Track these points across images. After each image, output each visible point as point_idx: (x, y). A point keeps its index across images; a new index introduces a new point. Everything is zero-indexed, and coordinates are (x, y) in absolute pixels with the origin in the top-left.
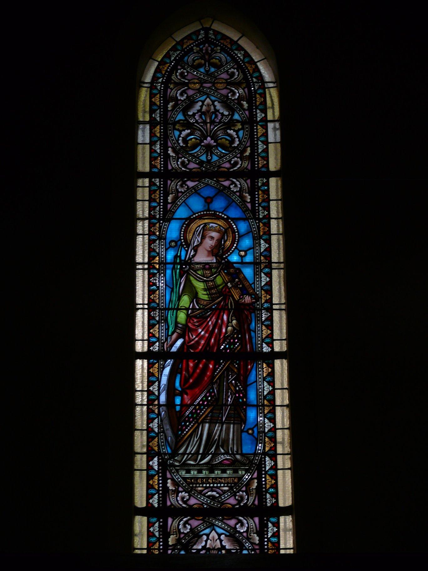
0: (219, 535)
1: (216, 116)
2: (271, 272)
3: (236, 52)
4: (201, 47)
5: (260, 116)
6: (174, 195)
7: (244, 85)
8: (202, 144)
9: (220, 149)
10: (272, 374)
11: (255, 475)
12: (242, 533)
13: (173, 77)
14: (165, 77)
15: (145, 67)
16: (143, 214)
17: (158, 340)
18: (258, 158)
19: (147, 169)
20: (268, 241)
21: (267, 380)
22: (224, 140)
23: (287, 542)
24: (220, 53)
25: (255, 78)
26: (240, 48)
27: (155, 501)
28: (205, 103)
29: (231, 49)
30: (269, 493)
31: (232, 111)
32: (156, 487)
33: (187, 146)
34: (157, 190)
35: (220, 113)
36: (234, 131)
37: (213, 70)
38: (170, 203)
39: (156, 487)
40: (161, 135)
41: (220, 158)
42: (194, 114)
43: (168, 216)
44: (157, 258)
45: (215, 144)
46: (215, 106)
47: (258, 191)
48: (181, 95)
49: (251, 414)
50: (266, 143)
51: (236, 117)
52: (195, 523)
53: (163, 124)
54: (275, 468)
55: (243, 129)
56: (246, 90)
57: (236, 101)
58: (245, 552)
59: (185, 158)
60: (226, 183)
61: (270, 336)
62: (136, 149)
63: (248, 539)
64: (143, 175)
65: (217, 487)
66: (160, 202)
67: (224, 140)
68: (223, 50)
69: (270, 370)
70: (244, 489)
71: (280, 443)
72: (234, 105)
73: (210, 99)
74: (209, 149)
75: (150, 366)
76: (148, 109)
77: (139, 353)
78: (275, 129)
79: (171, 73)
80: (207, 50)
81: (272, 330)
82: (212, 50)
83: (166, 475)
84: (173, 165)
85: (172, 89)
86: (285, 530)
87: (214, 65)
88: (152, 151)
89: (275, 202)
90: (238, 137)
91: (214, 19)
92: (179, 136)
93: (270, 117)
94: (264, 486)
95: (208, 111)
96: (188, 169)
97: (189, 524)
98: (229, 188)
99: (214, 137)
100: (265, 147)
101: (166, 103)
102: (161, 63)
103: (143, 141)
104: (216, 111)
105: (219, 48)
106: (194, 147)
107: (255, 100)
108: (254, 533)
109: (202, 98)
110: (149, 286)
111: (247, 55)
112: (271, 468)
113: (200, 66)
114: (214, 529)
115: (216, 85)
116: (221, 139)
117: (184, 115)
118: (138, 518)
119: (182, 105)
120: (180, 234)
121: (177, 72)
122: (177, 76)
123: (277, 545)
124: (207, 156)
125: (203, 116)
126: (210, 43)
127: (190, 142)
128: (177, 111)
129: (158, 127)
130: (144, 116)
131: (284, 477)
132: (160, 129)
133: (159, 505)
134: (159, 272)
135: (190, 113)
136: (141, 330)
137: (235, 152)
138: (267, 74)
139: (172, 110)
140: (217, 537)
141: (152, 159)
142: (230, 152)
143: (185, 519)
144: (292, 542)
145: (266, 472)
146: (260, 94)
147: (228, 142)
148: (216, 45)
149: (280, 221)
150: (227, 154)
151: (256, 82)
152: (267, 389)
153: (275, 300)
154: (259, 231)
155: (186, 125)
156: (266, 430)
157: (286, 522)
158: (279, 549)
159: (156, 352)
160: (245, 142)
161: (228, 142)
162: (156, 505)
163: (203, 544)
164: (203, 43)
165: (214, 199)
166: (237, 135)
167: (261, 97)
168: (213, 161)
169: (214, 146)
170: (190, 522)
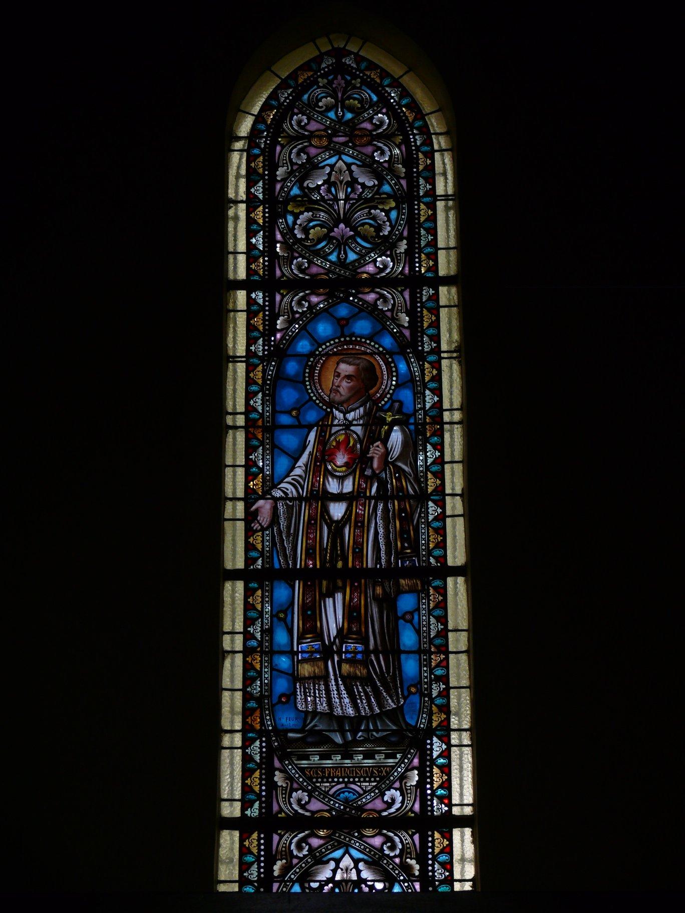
0: (356, 862)
4: (331, 78)
5: (423, 186)
6: (284, 861)
7: (399, 139)
12: (392, 858)
14: (268, 136)
18: (433, 866)
19: (240, 565)
22: (367, 227)
23: (465, 872)
28: (342, 865)
29: (381, 85)
30: (438, 766)
32: (255, 851)
33: (307, 238)
37: (349, 116)
39: (255, 851)
40: (264, 222)
45: (352, 233)
46: (359, 872)
48: (299, 303)
58: (397, 889)
61: (448, 850)
63: (395, 320)
64: (235, 575)
67: (367, 227)
72: (383, 171)
75: (249, 592)
76: (243, 172)
77: (229, 570)
78: (447, 209)
81: (440, 396)
83: (275, 235)
85: (283, 147)
86: (463, 860)
87: (351, 109)
89: (444, 251)
90: (389, 220)
92: (295, 223)
93: (440, 190)
96: (307, 811)
97: (307, 844)
98: (375, 304)
105: (359, 80)
107: (416, 169)
108: (411, 859)
109: (333, 160)
114: (340, 158)
121: (291, 119)
122: (292, 125)
123: (442, 560)
124: (339, 253)
125: (333, 190)
127: (312, 231)
129: (261, 208)
130: (232, 722)
131: (454, 527)
132: (264, 212)
134: (262, 390)
140: (345, 168)
141: (252, 159)
143: (300, 836)
144: (468, 719)
145: (428, 524)
146: (440, 767)
148: (355, 77)
152: (435, 627)
157: (463, 842)
158: (450, 805)
159: (255, 818)
161: (372, 229)
165: (351, 321)
166: (387, 217)
167: (433, 368)
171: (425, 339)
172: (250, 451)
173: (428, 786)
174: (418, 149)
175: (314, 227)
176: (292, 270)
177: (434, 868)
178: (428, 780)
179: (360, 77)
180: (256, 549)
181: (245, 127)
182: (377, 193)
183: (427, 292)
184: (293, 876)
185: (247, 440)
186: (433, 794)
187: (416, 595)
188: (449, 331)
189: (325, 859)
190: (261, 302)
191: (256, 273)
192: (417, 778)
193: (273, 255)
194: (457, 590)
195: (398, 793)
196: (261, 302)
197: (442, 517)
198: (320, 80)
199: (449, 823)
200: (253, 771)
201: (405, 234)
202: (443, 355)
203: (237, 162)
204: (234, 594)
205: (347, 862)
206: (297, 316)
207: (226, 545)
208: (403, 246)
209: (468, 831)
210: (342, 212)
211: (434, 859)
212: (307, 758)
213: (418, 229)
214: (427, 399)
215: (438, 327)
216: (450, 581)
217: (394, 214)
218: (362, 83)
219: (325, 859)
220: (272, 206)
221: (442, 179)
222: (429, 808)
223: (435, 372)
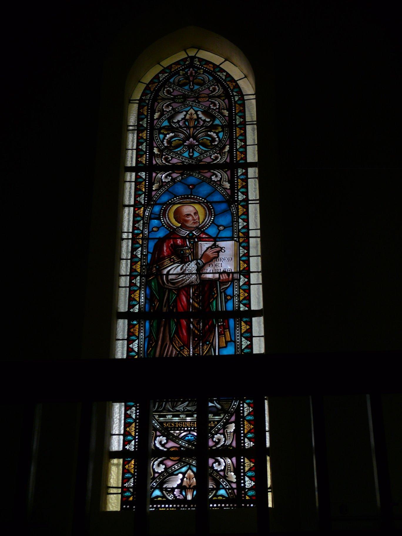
1: (199, 123)
4: (186, 70)
13: (160, 94)
16: (131, 164)
18: (237, 180)
21: (242, 245)
23: (259, 347)
24: (203, 74)
25: (236, 92)
28: (189, 113)
31: (213, 118)
33: (171, 146)
34: (140, 234)
35: (202, 120)
37: (196, 87)
42: (178, 122)
45: (197, 143)
46: (198, 115)
47: (238, 185)
51: (217, 122)
52: (169, 463)
53: (149, 131)
54: (248, 284)
57: (217, 110)
59: (170, 88)
60: (208, 175)
69: (245, 210)
74: (191, 147)
77: (115, 458)
79: (159, 90)
80: (191, 73)
84: (156, 161)
85: (159, 103)
87: (198, 84)
91: (199, 48)
92: (164, 138)
94: (242, 471)
95: (191, 119)
96: (165, 448)
99: (195, 138)
101: (153, 113)
104: (199, 118)
105: (202, 70)
109: (187, 109)
112: (245, 284)
113: (185, 84)
116: (202, 139)
117: (169, 122)
119: (160, 479)
122: (164, 93)
124: (190, 152)
133: (135, 448)
135: (175, 121)
136: (123, 296)
137: (216, 150)
139: (158, 119)
140: (194, 112)
141: (126, 443)
142: (211, 149)
147: (209, 141)
148: (200, 69)
149: (257, 180)
150: (208, 151)
151: (236, 95)
154: (238, 211)
155: (170, 129)
160: (224, 141)
161: (209, 141)
169: (196, 145)
170: (165, 462)
172: (128, 408)
173: (242, 432)
175: (175, 141)
177: (244, 441)
178: (242, 467)
179: (203, 69)
181: (137, 95)
183: (240, 171)
184: (154, 484)
185: (136, 189)
188: (254, 192)
189: (175, 473)
190: (144, 177)
191: (141, 162)
193: (152, 154)
195: (222, 436)
196: (144, 177)
198: (181, 72)
199: (246, 165)
200: (130, 424)
201: (228, 143)
202: (250, 202)
203: (134, 109)
206: (164, 184)
208: (227, 148)
209: (262, 318)
211: (245, 436)
212: (164, 416)
215: (249, 300)
216: (254, 319)
217: (221, 135)
219: (175, 473)
222: (242, 408)
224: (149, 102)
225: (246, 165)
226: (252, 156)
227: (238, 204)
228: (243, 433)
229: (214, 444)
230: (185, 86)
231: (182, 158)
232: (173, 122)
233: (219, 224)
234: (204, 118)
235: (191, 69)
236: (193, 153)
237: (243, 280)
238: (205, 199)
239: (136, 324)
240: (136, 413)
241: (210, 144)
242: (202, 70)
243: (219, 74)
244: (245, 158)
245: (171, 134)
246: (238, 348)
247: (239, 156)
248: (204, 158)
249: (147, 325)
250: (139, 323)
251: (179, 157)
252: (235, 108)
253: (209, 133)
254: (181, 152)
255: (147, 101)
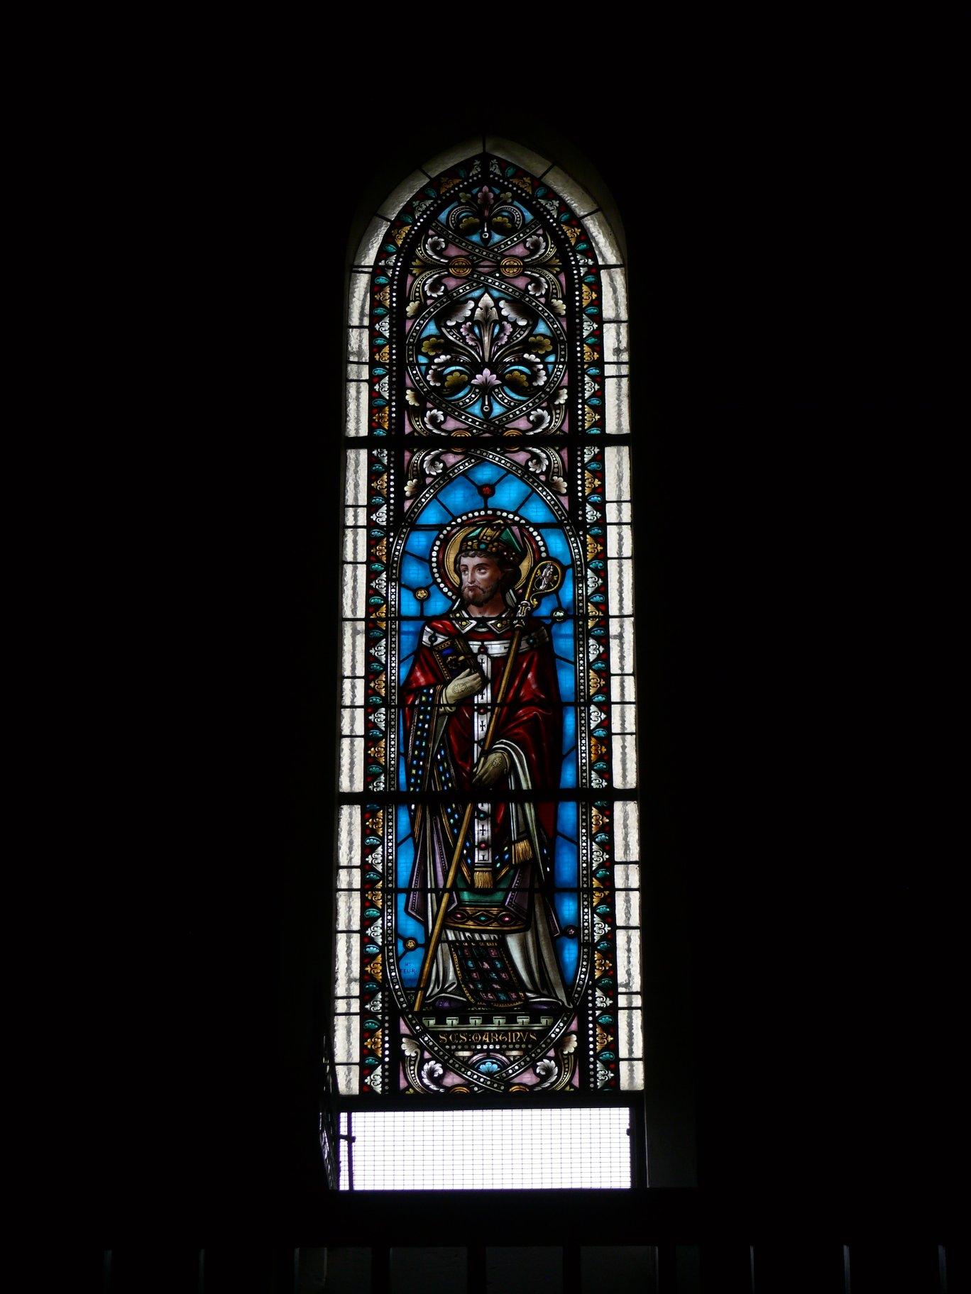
0: (496, 301)
2: (606, 565)
3: (543, 202)
4: (475, 191)
8: (474, 382)
9: (507, 390)
10: (608, 829)
11: (574, 1026)
15: (360, 241)
17: (385, 770)
18: (583, 474)
20: (602, 573)
21: (592, 532)
26: (551, 195)
27: (376, 1080)
31: (533, 318)
36: (537, 356)
37: (497, 238)
38: (409, 498)
41: (509, 410)
43: (403, 522)
44: (384, 608)
45: (499, 382)
46: (499, 310)
48: (432, 463)
49: (568, 908)
50: (598, 319)
55: (554, 352)
56: (563, 278)
57: (543, 300)
62: (340, 745)
63: (549, 305)
65: (495, 1050)
66: (384, 1056)
68: (516, 197)
70: (552, 1053)
71: (615, 637)
73: (491, 296)
82: (497, 198)
85: (415, 277)
87: (500, 229)
88: (373, 395)
96: (445, 258)
99: (495, 367)
100: (597, 387)
102: (397, 225)
103: (350, 896)
106: (458, 387)
109: (476, 294)
110: (364, 836)
111: (564, 207)
113: (473, 229)
115: (502, 270)
117: (439, 327)
118: (345, 810)
120: (433, 574)
121: (425, 242)
126: (492, 184)
128: (424, 319)
137: (540, 398)
138: (608, 252)
140: (491, 303)
145: (584, 467)
147: (524, 377)
148: (504, 189)
150: (524, 402)
152: (598, 857)
153: (611, 494)
154: (585, 551)
156: (596, 938)
162: (379, 1089)
163: (468, 313)
164: (479, 184)
165: (497, 488)
167: (594, 351)
168: (492, 242)
169: (497, 386)
170: (443, 457)
171: (587, 379)
174: (581, 280)
175: (451, 373)
176: (424, 424)
180: (378, 694)
182: (530, 334)
186: (596, 1056)
187: (575, 895)
192: (575, 1044)
193: (402, 404)
194: (626, 817)
197: (613, 1010)
200: (381, 347)
201: (565, 382)
204: (350, 820)
205: (487, 298)
207: (345, 596)
208: (564, 397)
210: (487, 355)
213: (580, 364)
214: (591, 650)
218: (513, 198)
220: (398, 355)
221: (617, 641)
223: (594, 296)
224: (393, 274)
225: (612, 795)
226: (617, 418)
227: (586, 532)
228: (594, 1049)
229: (530, 426)
230: (474, 233)
231: (467, 418)
232: (446, 327)
233: (544, 600)
234: (512, 316)
235: (485, 188)
236: (490, 405)
237: (601, 1000)
238: (515, 514)
239: (385, 285)
240: (391, 298)
241: (526, 384)
242: (509, 194)
243: (543, 202)
244: (601, 423)
245: (443, 358)
246: (582, 725)
247: (590, 417)
248: (516, 418)
249: (404, 819)
250: (386, 813)
251: (460, 415)
252: (580, 295)
253: (526, 356)
254: (465, 403)
255: (390, 273)
